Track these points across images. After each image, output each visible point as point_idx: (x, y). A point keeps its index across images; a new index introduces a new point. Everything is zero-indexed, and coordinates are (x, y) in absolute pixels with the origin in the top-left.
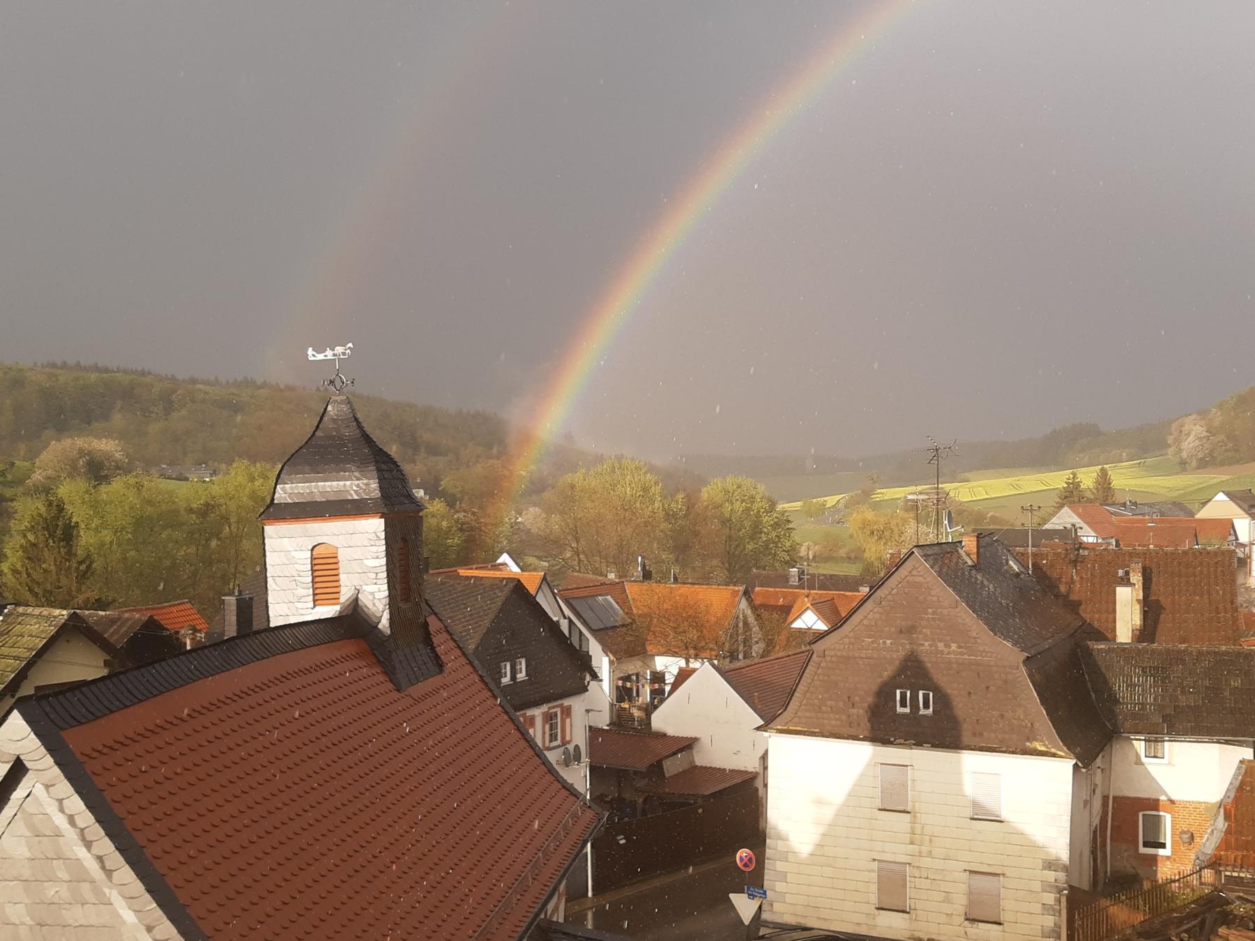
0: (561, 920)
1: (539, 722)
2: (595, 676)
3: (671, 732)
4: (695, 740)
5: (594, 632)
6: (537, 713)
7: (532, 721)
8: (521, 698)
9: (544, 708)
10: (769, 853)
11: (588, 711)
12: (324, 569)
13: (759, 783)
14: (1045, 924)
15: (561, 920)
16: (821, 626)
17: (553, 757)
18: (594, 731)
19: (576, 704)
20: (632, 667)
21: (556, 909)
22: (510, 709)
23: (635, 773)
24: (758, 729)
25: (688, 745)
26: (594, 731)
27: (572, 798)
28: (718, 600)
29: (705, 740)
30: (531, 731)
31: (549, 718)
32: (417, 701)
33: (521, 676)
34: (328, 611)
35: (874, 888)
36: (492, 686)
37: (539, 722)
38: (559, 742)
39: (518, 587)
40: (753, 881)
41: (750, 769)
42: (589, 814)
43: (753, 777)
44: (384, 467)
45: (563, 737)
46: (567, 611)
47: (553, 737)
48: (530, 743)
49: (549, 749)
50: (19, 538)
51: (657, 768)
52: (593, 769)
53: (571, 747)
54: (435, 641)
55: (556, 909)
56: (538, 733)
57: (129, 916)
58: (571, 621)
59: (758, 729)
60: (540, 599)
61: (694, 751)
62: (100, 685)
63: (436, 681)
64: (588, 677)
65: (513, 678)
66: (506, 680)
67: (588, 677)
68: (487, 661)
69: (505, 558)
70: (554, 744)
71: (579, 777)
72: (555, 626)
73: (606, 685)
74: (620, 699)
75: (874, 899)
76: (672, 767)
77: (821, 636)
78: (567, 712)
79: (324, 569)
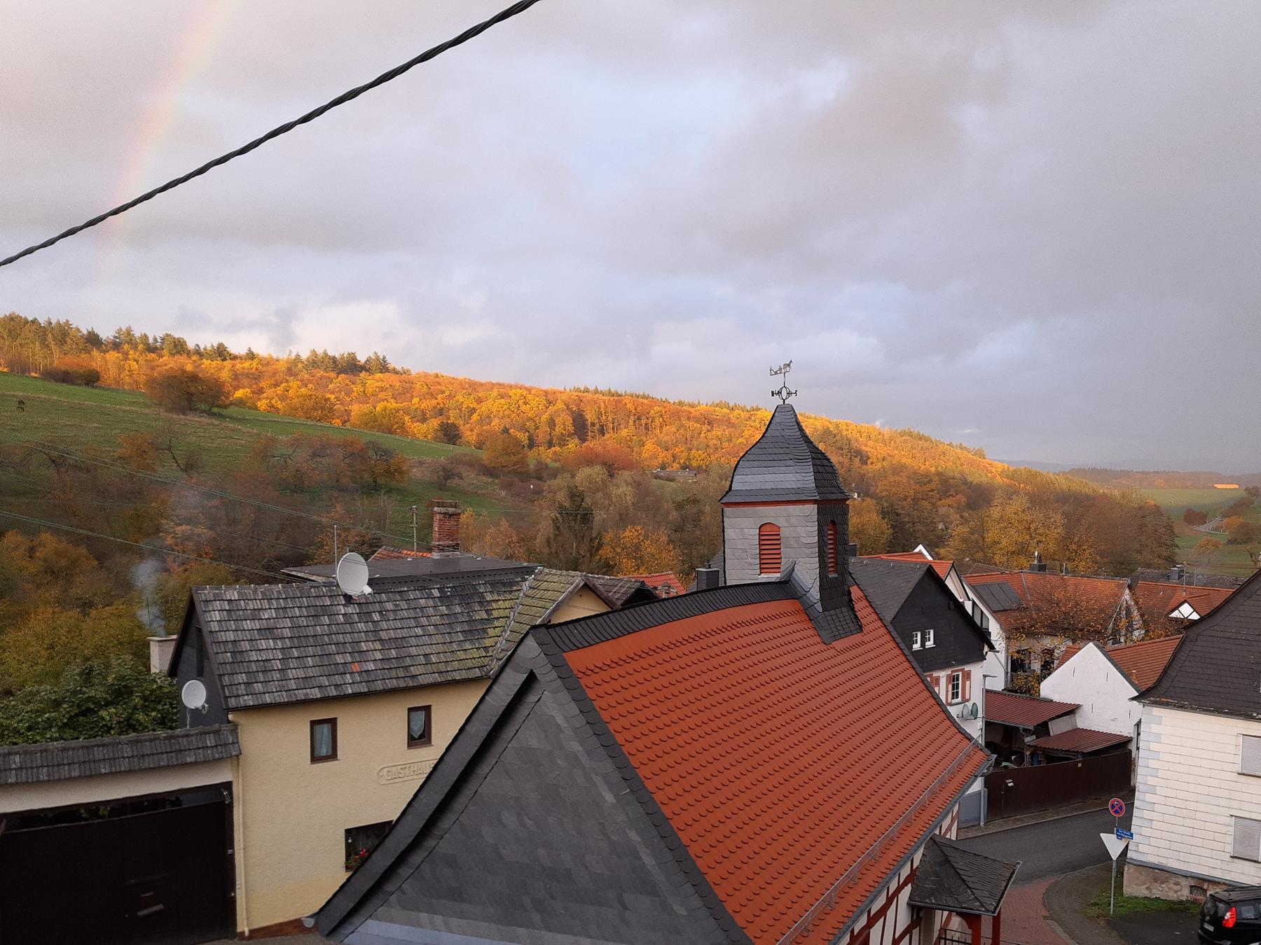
0: (954, 838)
1: (943, 682)
2: (992, 648)
3: (1056, 699)
4: (1078, 707)
5: (994, 612)
6: (943, 675)
7: (937, 680)
8: (927, 662)
9: (949, 672)
10: (1137, 803)
11: (985, 676)
12: (769, 540)
13: (1133, 747)
14: (990, 457)
15: (954, 838)
16: (1195, 617)
17: (954, 711)
18: (988, 693)
19: (977, 670)
20: (1025, 644)
21: (949, 829)
22: (919, 670)
23: (1025, 730)
24: (1133, 699)
25: (1071, 710)
26: (988, 693)
27: (966, 741)
28: (1102, 589)
29: (1086, 708)
30: (936, 689)
31: (953, 680)
32: (840, 653)
33: (930, 644)
34: (774, 577)
35: (1230, 839)
36: (906, 652)
37: (943, 682)
38: (959, 700)
39: (930, 573)
40: (1124, 827)
41: (1125, 734)
42: (980, 754)
43: (1129, 740)
44: (818, 462)
45: (963, 697)
46: (971, 595)
47: (955, 695)
48: (935, 697)
49: (951, 705)
50: (670, 456)
51: (1042, 729)
52: (988, 725)
53: (969, 705)
54: (857, 607)
55: (949, 829)
56: (943, 690)
57: (609, 798)
58: (974, 603)
59: (1133, 699)
60: (949, 583)
61: (1077, 715)
62: (582, 623)
63: (857, 638)
64: (986, 649)
65: (923, 644)
66: (917, 647)
67: (986, 649)
68: (902, 628)
69: (920, 548)
70: (955, 701)
71: (975, 729)
72: (960, 607)
73: (1002, 656)
74: (1014, 669)
75: (1229, 849)
76: (1056, 728)
77: (1194, 622)
78: (967, 676)
79: (769, 540)
